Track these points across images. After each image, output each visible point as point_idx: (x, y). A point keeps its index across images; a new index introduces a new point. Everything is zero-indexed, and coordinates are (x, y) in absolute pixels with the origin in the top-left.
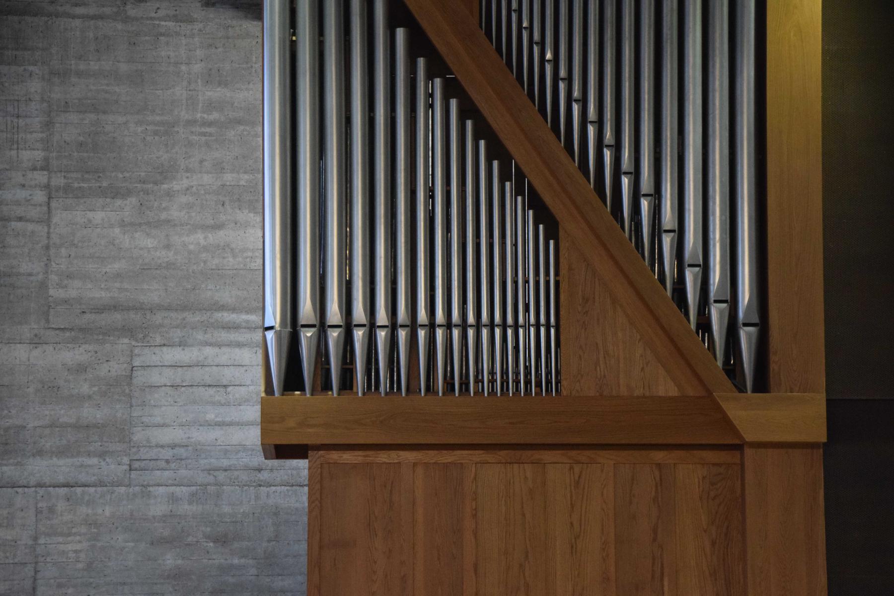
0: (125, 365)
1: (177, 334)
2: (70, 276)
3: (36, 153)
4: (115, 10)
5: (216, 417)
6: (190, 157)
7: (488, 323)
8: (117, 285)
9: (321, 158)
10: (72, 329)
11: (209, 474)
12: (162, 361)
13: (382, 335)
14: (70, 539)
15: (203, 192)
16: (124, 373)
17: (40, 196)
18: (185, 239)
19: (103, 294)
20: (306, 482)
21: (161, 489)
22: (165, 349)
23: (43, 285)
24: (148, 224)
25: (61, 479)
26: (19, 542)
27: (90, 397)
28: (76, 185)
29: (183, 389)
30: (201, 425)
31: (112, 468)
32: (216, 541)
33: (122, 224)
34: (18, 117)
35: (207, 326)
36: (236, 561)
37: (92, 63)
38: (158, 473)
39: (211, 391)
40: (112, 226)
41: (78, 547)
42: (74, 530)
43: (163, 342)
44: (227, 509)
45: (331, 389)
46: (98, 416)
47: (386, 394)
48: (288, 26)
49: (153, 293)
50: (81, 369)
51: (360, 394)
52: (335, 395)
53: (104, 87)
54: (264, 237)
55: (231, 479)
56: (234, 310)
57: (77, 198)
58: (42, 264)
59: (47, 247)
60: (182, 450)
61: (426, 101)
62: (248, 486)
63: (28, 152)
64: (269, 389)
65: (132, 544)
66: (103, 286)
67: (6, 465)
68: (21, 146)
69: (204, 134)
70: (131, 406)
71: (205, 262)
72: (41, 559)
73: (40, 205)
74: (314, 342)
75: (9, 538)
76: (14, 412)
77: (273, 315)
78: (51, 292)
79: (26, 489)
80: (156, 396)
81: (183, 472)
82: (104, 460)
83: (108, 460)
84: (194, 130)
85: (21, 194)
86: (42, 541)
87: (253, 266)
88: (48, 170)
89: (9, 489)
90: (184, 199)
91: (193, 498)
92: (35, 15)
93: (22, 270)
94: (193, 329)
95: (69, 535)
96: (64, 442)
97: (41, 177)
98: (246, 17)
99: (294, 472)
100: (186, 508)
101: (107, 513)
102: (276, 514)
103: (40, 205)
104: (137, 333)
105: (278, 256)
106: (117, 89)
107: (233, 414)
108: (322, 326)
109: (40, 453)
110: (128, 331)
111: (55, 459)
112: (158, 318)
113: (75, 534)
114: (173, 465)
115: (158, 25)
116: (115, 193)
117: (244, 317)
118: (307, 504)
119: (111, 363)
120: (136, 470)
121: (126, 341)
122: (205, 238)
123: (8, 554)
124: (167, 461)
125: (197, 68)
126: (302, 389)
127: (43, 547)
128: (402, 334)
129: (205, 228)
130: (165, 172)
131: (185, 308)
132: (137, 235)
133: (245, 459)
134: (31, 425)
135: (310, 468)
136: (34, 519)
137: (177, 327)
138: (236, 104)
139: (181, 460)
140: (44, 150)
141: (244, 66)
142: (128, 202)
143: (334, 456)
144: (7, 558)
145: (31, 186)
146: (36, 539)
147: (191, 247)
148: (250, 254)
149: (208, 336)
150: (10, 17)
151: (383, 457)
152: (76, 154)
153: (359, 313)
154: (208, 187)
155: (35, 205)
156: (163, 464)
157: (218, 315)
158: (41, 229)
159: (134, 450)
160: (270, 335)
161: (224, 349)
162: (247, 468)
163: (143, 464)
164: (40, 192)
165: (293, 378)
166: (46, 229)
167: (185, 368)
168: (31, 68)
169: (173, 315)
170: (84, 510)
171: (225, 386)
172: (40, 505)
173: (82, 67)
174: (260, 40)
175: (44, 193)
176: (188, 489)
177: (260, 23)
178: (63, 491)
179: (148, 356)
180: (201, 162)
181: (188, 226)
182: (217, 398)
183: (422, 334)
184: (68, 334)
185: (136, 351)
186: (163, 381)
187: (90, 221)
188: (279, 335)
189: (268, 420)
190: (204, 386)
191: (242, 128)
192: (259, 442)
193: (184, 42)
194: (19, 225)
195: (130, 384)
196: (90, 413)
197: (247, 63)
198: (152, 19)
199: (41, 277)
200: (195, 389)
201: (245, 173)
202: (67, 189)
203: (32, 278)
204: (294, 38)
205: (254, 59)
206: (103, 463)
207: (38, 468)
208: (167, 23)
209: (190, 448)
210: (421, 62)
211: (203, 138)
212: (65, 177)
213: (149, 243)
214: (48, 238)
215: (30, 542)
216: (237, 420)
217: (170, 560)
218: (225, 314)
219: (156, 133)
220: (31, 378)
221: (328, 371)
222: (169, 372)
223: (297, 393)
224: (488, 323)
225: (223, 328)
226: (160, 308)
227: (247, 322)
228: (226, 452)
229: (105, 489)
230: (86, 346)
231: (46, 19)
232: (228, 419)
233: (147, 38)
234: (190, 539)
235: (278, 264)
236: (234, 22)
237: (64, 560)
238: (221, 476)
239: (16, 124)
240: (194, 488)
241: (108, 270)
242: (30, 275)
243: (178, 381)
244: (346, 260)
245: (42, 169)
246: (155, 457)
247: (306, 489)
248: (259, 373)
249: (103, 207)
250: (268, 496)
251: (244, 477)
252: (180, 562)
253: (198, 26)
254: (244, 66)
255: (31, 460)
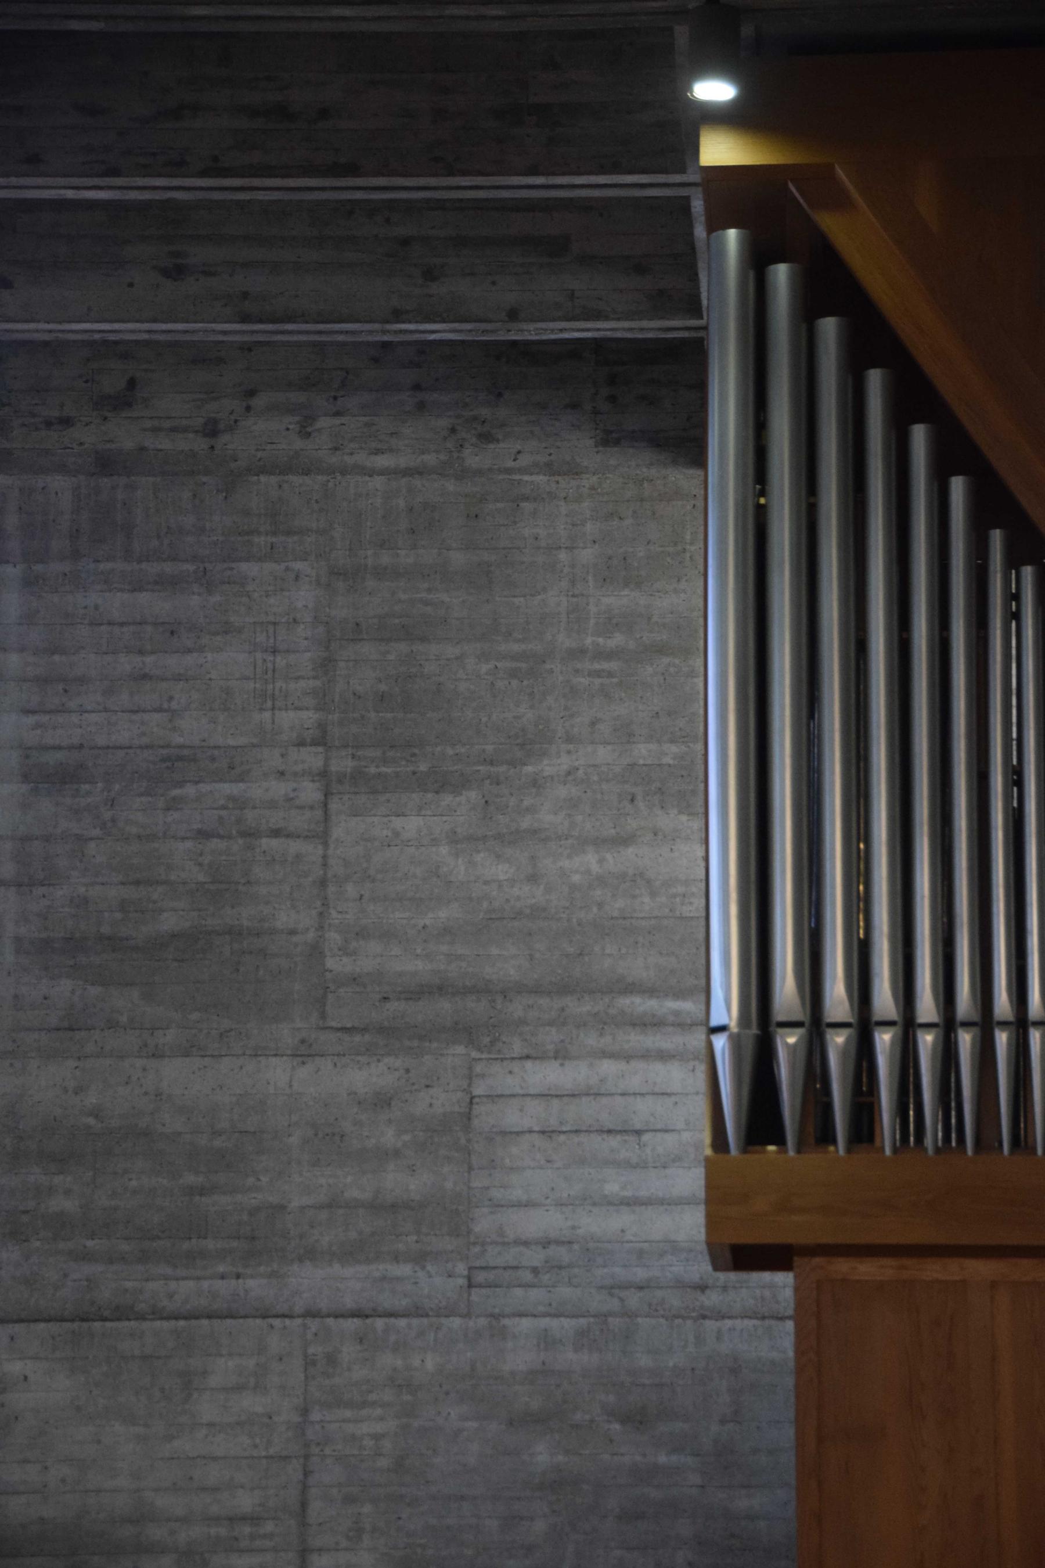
0: (460, 1094)
1: (550, 1037)
2: (362, 934)
3: (304, 714)
4: (443, 457)
5: (623, 1188)
6: (572, 716)
7: (976, 1017)
8: (444, 948)
9: (811, 715)
10: (364, 1030)
11: (611, 1295)
12: (526, 1086)
13: (927, 1040)
14: (365, 1412)
15: (596, 778)
16: (457, 1109)
17: (310, 792)
18: (566, 863)
19: (420, 965)
20: (790, 1312)
21: (525, 1323)
22: (529, 1064)
23: (316, 951)
24: (499, 837)
25: (349, 1302)
26: (275, 1419)
27: (397, 1153)
28: (373, 770)
29: (562, 1138)
30: (594, 1204)
31: (436, 1283)
32: (625, 1419)
33: (453, 839)
34: (275, 652)
35: (603, 1022)
36: (662, 1459)
37: (402, 553)
38: (519, 1292)
39: (614, 1141)
40: (435, 842)
41: (379, 1428)
42: (373, 1397)
43: (526, 1051)
44: (644, 1361)
45: (834, 1141)
46: (412, 1187)
47: (938, 1150)
48: (750, 480)
49: (506, 963)
50: (382, 1101)
51: (888, 1151)
52: (842, 1151)
53: (424, 595)
54: (707, 859)
55: (650, 1305)
56: (651, 991)
57: (375, 792)
58: (314, 912)
59: (323, 883)
60: (562, 1250)
61: (1006, 606)
62: (684, 1318)
63: (291, 714)
64: (719, 1141)
65: (474, 1424)
66: (419, 951)
67: (252, 1277)
68: (278, 704)
69: (598, 674)
70: (470, 1169)
71: (600, 905)
72: (315, 1450)
73: (312, 808)
74: (802, 1054)
75: (259, 1409)
76: (264, 1179)
77: (725, 1004)
78: (330, 963)
79: (287, 1321)
80: (514, 1150)
81: (565, 1292)
82: (423, 1268)
83: (429, 1268)
84: (579, 666)
85: (279, 789)
86: (315, 1416)
87: (687, 911)
88: (325, 744)
89: (258, 1321)
90: (562, 791)
91: (582, 1339)
92: (307, 473)
93: (279, 925)
94: (578, 1027)
95: (364, 1404)
96: (353, 1235)
97: (312, 758)
98: (675, 462)
99: (767, 1293)
100: (569, 1358)
101: (430, 1365)
102: (735, 1371)
103: (312, 808)
104: (481, 1035)
105: (734, 896)
106: (445, 597)
107: (653, 1184)
108: (816, 1026)
109: (310, 1255)
110: (464, 1031)
111: (337, 1266)
112: (516, 1008)
113: (373, 1404)
114: (545, 1278)
115: (519, 482)
116: (442, 782)
117: (672, 1004)
118: (791, 1354)
119: (431, 1091)
120: (480, 1286)
121: (460, 1049)
122: (601, 861)
123: (258, 1441)
124: (535, 1271)
125: (587, 555)
126: (780, 1140)
127: (317, 1427)
128: (965, 1039)
129: (600, 842)
130: (530, 743)
131: (564, 989)
132: (479, 858)
133: (677, 1268)
134: (295, 1204)
135: (797, 1289)
136: (302, 1376)
137: (551, 1023)
138: (655, 619)
139: (560, 1267)
140: (317, 709)
141: (671, 549)
142: (462, 799)
143: (842, 1266)
144: (256, 1446)
145: (295, 774)
146: (305, 1412)
147: (576, 878)
148: (681, 889)
149: (608, 1039)
150: (263, 478)
151: (933, 1270)
152: (373, 715)
153: (884, 998)
154: (604, 769)
155: (301, 808)
156: (528, 1276)
157: (625, 1002)
158: (312, 851)
159: (477, 1249)
160: (720, 1042)
161: (639, 1065)
162: (680, 1284)
163: (491, 1276)
164: (311, 785)
165: (762, 1121)
166: (320, 851)
167: (565, 1099)
168: (298, 565)
169: (544, 1001)
170: (388, 1360)
171: (638, 1133)
172: (311, 1350)
173: (386, 559)
174: (700, 504)
175: (317, 784)
176: (573, 1322)
177: (700, 472)
178: (351, 1324)
179: (500, 1078)
180: (593, 724)
181: (570, 841)
182: (623, 1154)
183: (1002, 1039)
184: (357, 1038)
185: (478, 1068)
186: (526, 1123)
187: (397, 834)
188: (736, 1042)
189: (719, 1197)
190: (601, 1131)
191: (666, 660)
192: (702, 1237)
193: (564, 509)
194: (274, 843)
195: (467, 1128)
196: (397, 1182)
197: (676, 544)
198: (509, 471)
199: (311, 935)
200: (583, 1138)
201: (672, 741)
202: (357, 777)
203: (295, 939)
204: (762, 501)
205: (688, 537)
206: (421, 1274)
207: (309, 1282)
208: (534, 478)
209: (576, 1247)
210: (997, 537)
211: (598, 681)
212: (353, 756)
213: (502, 871)
214: (325, 865)
215: (297, 1419)
216: (661, 1194)
217: (543, 1455)
218: (638, 1000)
219: (513, 674)
220: (294, 1118)
221: (827, 1108)
222: (535, 1107)
223: (772, 1148)
224: (976, 1017)
225: (634, 1025)
226: (521, 989)
227: (677, 1013)
228: (641, 1253)
229: (425, 1321)
230: (388, 1060)
231: (325, 478)
232: (643, 1193)
233: (499, 505)
234: (578, 1416)
235: (734, 910)
236: (653, 472)
237: (356, 1452)
238: (634, 1300)
239: (270, 665)
240: (583, 1321)
241: (428, 922)
242: (293, 932)
243: (553, 1123)
244: (859, 904)
245: (315, 743)
246: (515, 1264)
247: (790, 1325)
248: (701, 1107)
249: (420, 808)
250: (719, 1337)
251: (675, 1301)
252: (561, 1458)
253: (588, 481)
254: (671, 549)
255: (295, 1267)
